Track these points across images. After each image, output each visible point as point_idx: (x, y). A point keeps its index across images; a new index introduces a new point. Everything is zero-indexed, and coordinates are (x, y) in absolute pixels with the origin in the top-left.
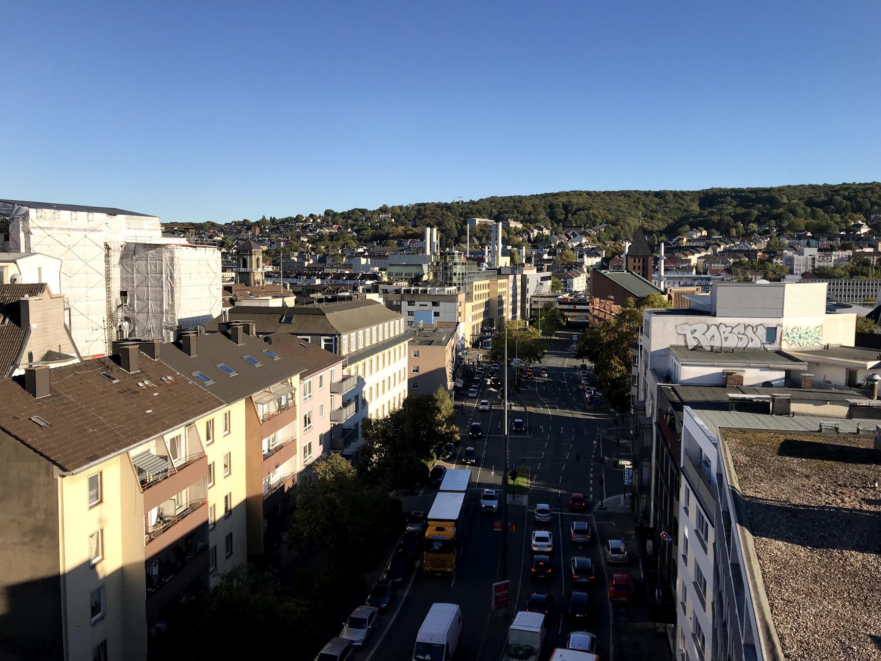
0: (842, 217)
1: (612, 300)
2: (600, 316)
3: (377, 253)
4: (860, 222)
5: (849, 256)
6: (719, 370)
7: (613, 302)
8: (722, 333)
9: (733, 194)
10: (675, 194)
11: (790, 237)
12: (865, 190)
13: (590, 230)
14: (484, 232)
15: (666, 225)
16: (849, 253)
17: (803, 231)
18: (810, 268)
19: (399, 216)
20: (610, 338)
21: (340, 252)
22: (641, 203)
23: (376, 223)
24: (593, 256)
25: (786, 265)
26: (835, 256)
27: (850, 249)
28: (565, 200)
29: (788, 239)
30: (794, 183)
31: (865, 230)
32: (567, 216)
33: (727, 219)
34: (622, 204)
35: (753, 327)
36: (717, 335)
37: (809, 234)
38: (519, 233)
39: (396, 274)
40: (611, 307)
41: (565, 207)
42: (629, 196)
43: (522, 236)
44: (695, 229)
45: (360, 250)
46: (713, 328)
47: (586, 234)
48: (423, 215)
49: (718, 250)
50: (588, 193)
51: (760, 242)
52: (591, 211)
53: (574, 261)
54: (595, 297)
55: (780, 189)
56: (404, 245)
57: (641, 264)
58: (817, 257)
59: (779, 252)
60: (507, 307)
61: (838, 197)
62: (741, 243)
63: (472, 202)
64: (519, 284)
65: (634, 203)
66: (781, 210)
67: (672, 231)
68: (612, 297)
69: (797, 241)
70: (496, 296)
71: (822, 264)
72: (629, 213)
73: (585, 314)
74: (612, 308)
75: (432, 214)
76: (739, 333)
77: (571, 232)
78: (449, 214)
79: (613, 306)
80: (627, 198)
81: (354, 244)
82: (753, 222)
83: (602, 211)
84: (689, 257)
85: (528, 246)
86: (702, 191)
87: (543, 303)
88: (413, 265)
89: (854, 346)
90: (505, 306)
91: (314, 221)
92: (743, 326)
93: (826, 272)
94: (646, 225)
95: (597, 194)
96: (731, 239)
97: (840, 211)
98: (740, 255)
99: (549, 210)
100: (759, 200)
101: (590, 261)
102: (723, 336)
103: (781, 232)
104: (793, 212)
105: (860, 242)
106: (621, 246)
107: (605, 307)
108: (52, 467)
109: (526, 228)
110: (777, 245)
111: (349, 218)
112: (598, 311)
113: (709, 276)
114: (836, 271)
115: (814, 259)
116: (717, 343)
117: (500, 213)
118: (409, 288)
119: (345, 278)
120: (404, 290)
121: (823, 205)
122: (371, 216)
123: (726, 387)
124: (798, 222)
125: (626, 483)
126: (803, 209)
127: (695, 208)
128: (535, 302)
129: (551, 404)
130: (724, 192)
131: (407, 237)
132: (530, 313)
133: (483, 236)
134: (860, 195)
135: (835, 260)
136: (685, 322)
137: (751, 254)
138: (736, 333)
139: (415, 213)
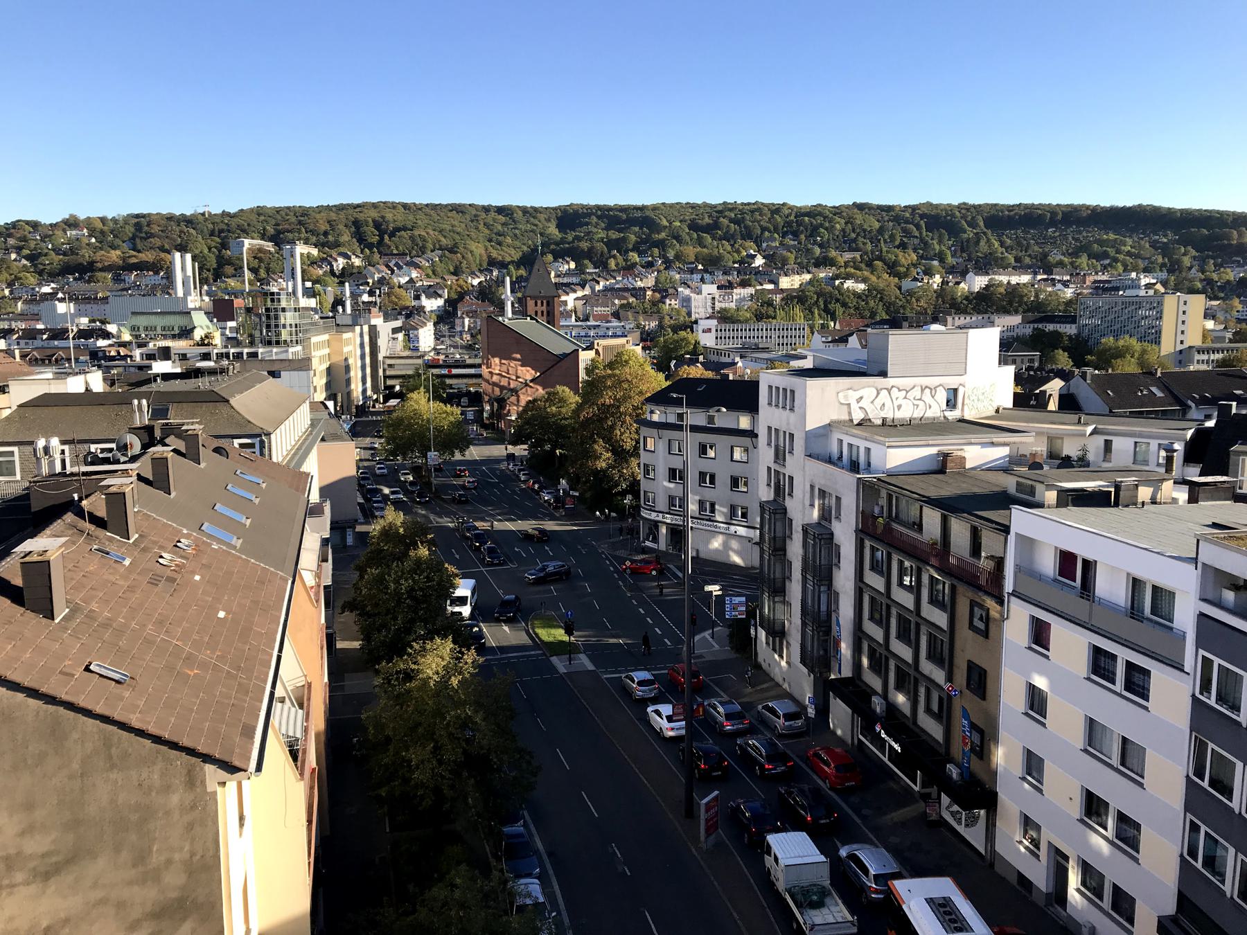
0: (732, 246)
1: (518, 360)
2: (502, 384)
3: (82, 295)
4: (752, 252)
5: (752, 294)
6: (934, 450)
7: (520, 363)
9: (599, 213)
10: (525, 210)
11: (680, 271)
12: (752, 212)
13: (419, 259)
14: (261, 260)
15: (521, 253)
16: (751, 290)
17: (693, 263)
18: (710, 310)
19: (102, 232)
20: (587, 413)
21: (7, 292)
22: (482, 223)
23: (63, 244)
24: (432, 297)
25: (683, 306)
26: (737, 294)
27: (750, 286)
28: (374, 214)
29: (679, 273)
30: (670, 200)
31: (759, 261)
32: (382, 239)
33: (600, 246)
34: (456, 223)
35: (931, 389)
38: (316, 263)
39: (146, 329)
40: (517, 370)
41: (377, 225)
43: (321, 267)
44: (561, 260)
45: (46, 289)
46: (884, 393)
47: (417, 266)
48: (146, 233)
49: (598, 288)
51: (647, 278)
52: (416, 233)
53: (408, 304)
54: (493, 357)
55: (655, 208)
56: (124, 280)
57: (544, 308)
58: (717, 297)
59: (671, 291)
60: (356, 374)
62: (623, 279)
63: (224, 214)
64: (366, 339)
66: (663, 235)
67: (528, 261)
68: (518, 356)
70: (341, 358)
71: (723, 305)
72: (468, 235)
73: (474, 381)
74: (519, 372)
75: (162, 231)
76: (914, 399)
77: (393, 262)
78: (192, 231)
79: (519, 368)
80: (461, 214)
81: (32, 279)
82: (632, 250)
83: (431, 232)
84: (563, 298)
85: (334, 282)
86: (559, 208)
87: (413, 367)
88: (174, 313)
89: (1011, 406)
90: (352, 374)
92: (920, 388)
93: (729, 315)
94: (494, 254)
95: (418, 208)
96: (610, 273)
97: (728, 237)
98: (626, 294)
99: (353, 229)
100: (631, 222)
101: (432, 304)
102: (896, 403)
103: (668, 264)
104: (678, 238)
105: (759, 276)
106: (466, 282)
107: (508, 370)
108: (202, 769)
109: (325, 256)
110: (668, 281)
111: (10, 235)
112: (498, 377)
113: (592, 323)
114: (741, 313)
115: (713, 299)
116: (888, 414)
117: (279, 232)
118: (224, 351)
119: (45, 337)
120: (217, 354)
121: (709, 229)
122: (51, 233)
123: (946, 472)
124: (687, 251)
125: (727, 617)
126: (688, 234)
127: (553, 230)
128: (390, 366)
129: (506, 514)
130: (587, 209)
131: (130, 268)
132: (385, 383)
133: (259, 267)
134: (748, 218)
135: (736, 300)
136: (849, 387)
137: (638, 293)
138: (912, 399)
139: (133, 230)
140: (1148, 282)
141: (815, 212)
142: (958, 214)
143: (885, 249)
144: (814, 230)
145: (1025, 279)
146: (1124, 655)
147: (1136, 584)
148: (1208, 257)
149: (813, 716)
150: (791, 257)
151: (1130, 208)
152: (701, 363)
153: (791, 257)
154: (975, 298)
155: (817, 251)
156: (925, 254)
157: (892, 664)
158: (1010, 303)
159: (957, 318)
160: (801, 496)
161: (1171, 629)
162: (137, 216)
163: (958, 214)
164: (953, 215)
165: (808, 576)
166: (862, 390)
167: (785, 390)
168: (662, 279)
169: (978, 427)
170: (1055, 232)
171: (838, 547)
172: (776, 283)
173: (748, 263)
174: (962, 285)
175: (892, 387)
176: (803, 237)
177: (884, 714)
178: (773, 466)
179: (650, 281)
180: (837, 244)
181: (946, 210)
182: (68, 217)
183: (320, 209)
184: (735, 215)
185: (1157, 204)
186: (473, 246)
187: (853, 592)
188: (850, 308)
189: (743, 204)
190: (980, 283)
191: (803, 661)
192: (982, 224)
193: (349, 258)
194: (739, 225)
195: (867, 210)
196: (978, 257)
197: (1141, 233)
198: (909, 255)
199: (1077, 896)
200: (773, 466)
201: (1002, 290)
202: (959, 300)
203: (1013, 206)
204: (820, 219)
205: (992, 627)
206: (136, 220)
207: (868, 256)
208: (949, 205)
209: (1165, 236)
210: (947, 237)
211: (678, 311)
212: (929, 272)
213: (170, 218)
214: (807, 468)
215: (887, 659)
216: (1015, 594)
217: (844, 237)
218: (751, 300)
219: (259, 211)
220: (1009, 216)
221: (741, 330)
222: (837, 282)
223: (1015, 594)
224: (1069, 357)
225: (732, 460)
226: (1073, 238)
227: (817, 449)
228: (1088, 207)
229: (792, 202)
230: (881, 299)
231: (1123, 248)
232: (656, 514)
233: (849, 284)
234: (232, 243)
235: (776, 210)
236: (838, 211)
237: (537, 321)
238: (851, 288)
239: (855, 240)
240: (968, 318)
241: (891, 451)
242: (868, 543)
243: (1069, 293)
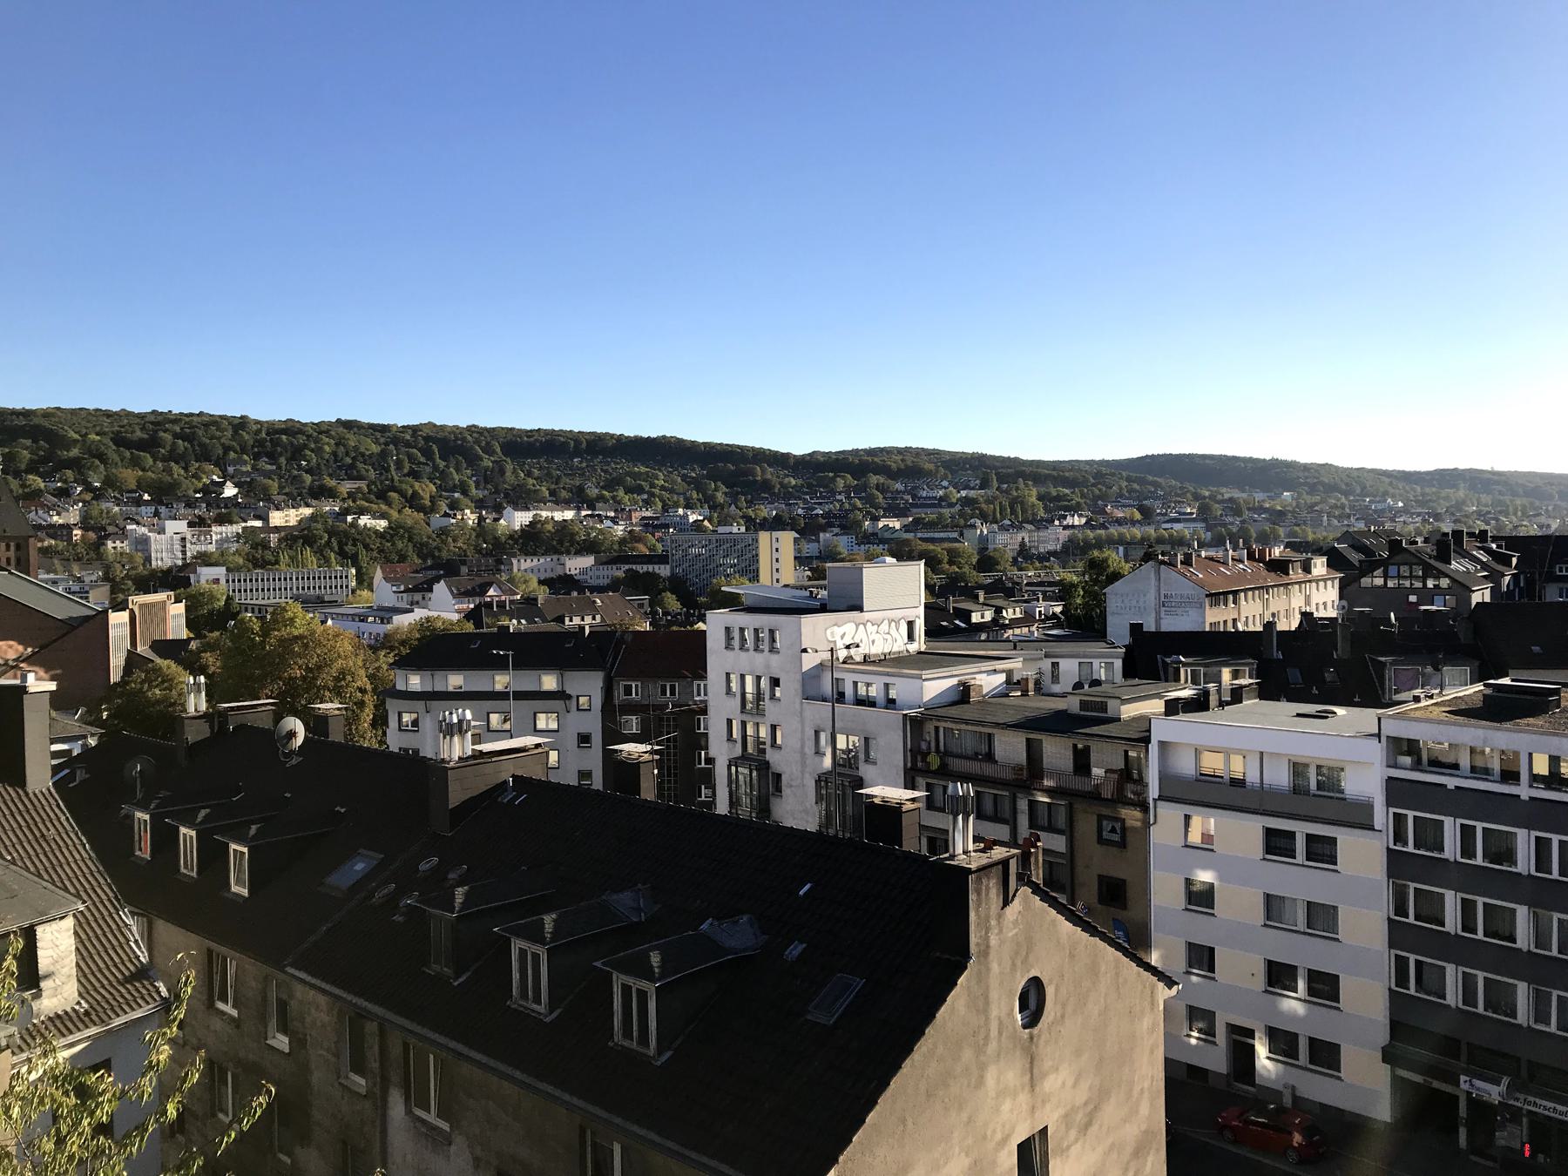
0: (186, 469)
5: (238, 533)
6: (954, 681)
11: (118, 502)
12: (206, 425)
16: (237, 528)
25: (137, 550)
26: (216, 533)
31: (230, 491)
37: (146, 497)
51: (68, 511)
58: (189, 537)
59: (111, 529)
61: (166, 435)
66: (75, 452)
69: (133, 509)
71: (198, 548)
104: (102, 457)
115: (183, 539)
121: (142, 445)
135: (217, 541)
138: (882, 632)
140: (695, 519)
141: (292, 428)
143: (396, 478)
144: (296, 453)
145: (569, 515)
146: (1301, 829)
147: (1298, 769)
148: (738, 493)
150: (274, 485)
151: (654, 439)
153: (274, 485)
154: (520, 537)
155: (308, 478)
156: (445, 487)
158: (561, 542)
159: (522, 561)
161: (1345, 799)
164: (464, 439)
168: (95, 513)
170: (581, 462)
172: (265, 519)
174: (502, 521)
175: (868, 621)
176: (283, 460)
179: (72, 515)
180: (330, 471)
181: (454, 433)
184: (182, 429)
188: (372, 550)
190: (520, 519)
192: (498, 450)
194: (190, 442)
195: (355, 429)
196: (506, 489)
198: (427, 486)
199: (1268, 1063)
201: (549, 527)
202: (503, 539)
203: (531, 431)
204: (302, 439)
205: (1130, 838)
207: (376, 486)
208: (457, 427)
209: (693, 470)
210: (465, 465)
211: (131, 557)
212: (454, 506)
216: (1161, 798)
217: (336, 461)
218: (238, 542)
220: (527, 442)
221: (280, 579)
222: (349, 519)
223: (1161, 798)
224: (677, 600)
226: (602, 470)
227: (812, 693)
228: (612, 436)
229: (254, 415)
230: (410, 539)
231: (656, 482)
233: (364, 520)
235: (241, 424)
238: (368, 525)
239: (352, 466)
240: (535, 560)
241: (925, 683)
243: (619, 530)
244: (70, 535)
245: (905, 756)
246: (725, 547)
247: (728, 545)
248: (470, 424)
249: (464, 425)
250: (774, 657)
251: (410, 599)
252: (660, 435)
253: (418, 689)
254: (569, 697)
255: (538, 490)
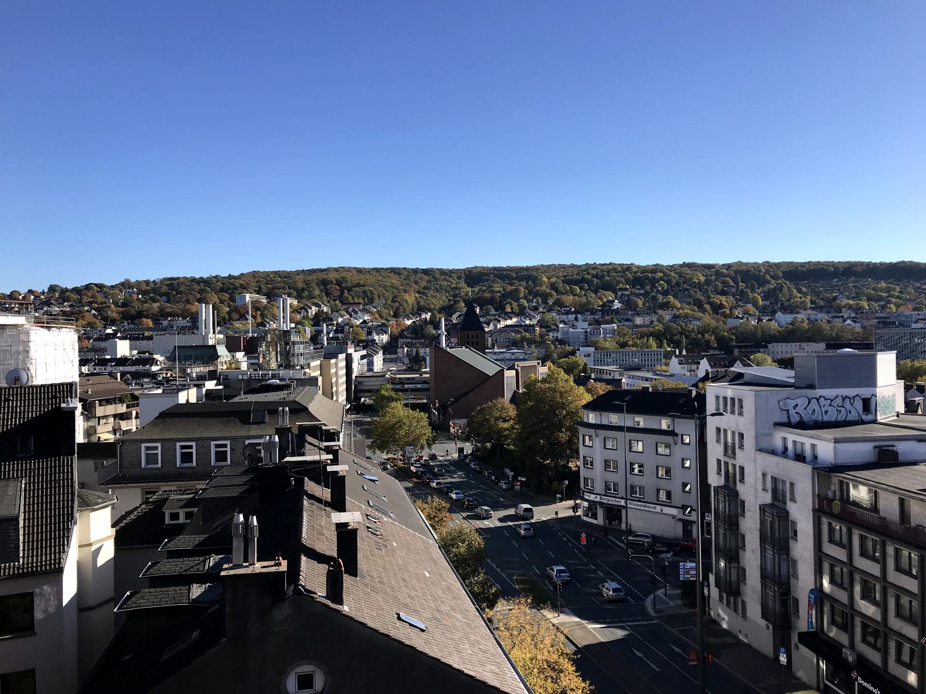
8: (822, 407)
11: (559, 313)
28: (337, 275)
35: (850, 398)
36: (817, 409)
38: (296, 310)
42: (399, 274)
43: (300, 313)
45: (109, 331)
47: (367, 311)
50: (377, 270)
63: (230, 277)
65: (405, 279)
77: (351, 309)
78: (208, 289)
91: (36, 297)
98: (520, 329)
102: (823, 410)
125: (681, 579)
138: (836, 406)
142: (763, 269)
144: (654, 282)
149: (785, 664)
151: (895, 264)
152: (593, 379)
157: (858, 621)
160: (753, 483)
162: (170, 279)
163: (763, 269)
164: (760, 271)
165: (767, 546)
166: (797, 400)
167: (733, 399)
169: (897, 428)
171: (794, 523)
173: (609, 306)
177: (856, 663)
178: (723, 459)
181: (753, 267)
182: (123, 281)
183: (298, 273)
185: (916, 260)
186: (407, 297)
187: (813, 561)
189: (600, 265)
191: (764, 616)
193: (319, 306)
197: (906, 282)
200: (723, 459)
203: (805, 263)
206: (169, 282)
208: (756, 263)
210: (757, 286)
213: (193, 280)
214: (758, 461)
215: (852, 616)
219: (254, 274)
225: (657, 454)
227: (764, 445)
228: (862, 264)
229: (637, 263)
232: (594, 496)
234: (237, 297)
235: (628, 268)
236: (673, 269)
237: (470, 349)
242: (825, 521)
244: (534, 331)
245: (813, 499)
246: (890, 345)
247: (893, 344)
248: (764, 260)
249: (760, 261)
250: (741, 418)
251: (689, 369)
252: (900, 260)
253: (593, 422)
254: (677, 435)
255: (805, 301)
